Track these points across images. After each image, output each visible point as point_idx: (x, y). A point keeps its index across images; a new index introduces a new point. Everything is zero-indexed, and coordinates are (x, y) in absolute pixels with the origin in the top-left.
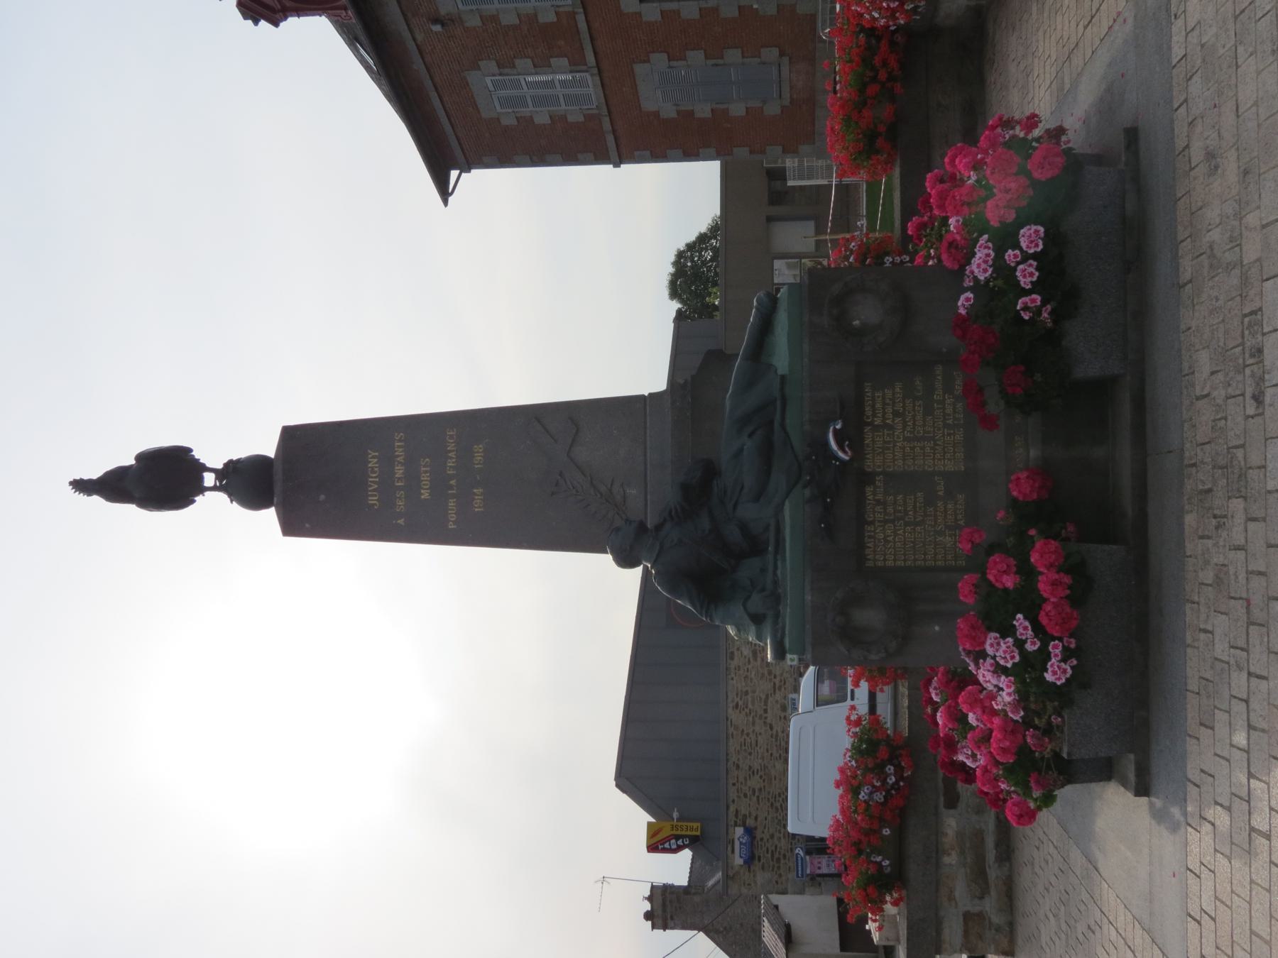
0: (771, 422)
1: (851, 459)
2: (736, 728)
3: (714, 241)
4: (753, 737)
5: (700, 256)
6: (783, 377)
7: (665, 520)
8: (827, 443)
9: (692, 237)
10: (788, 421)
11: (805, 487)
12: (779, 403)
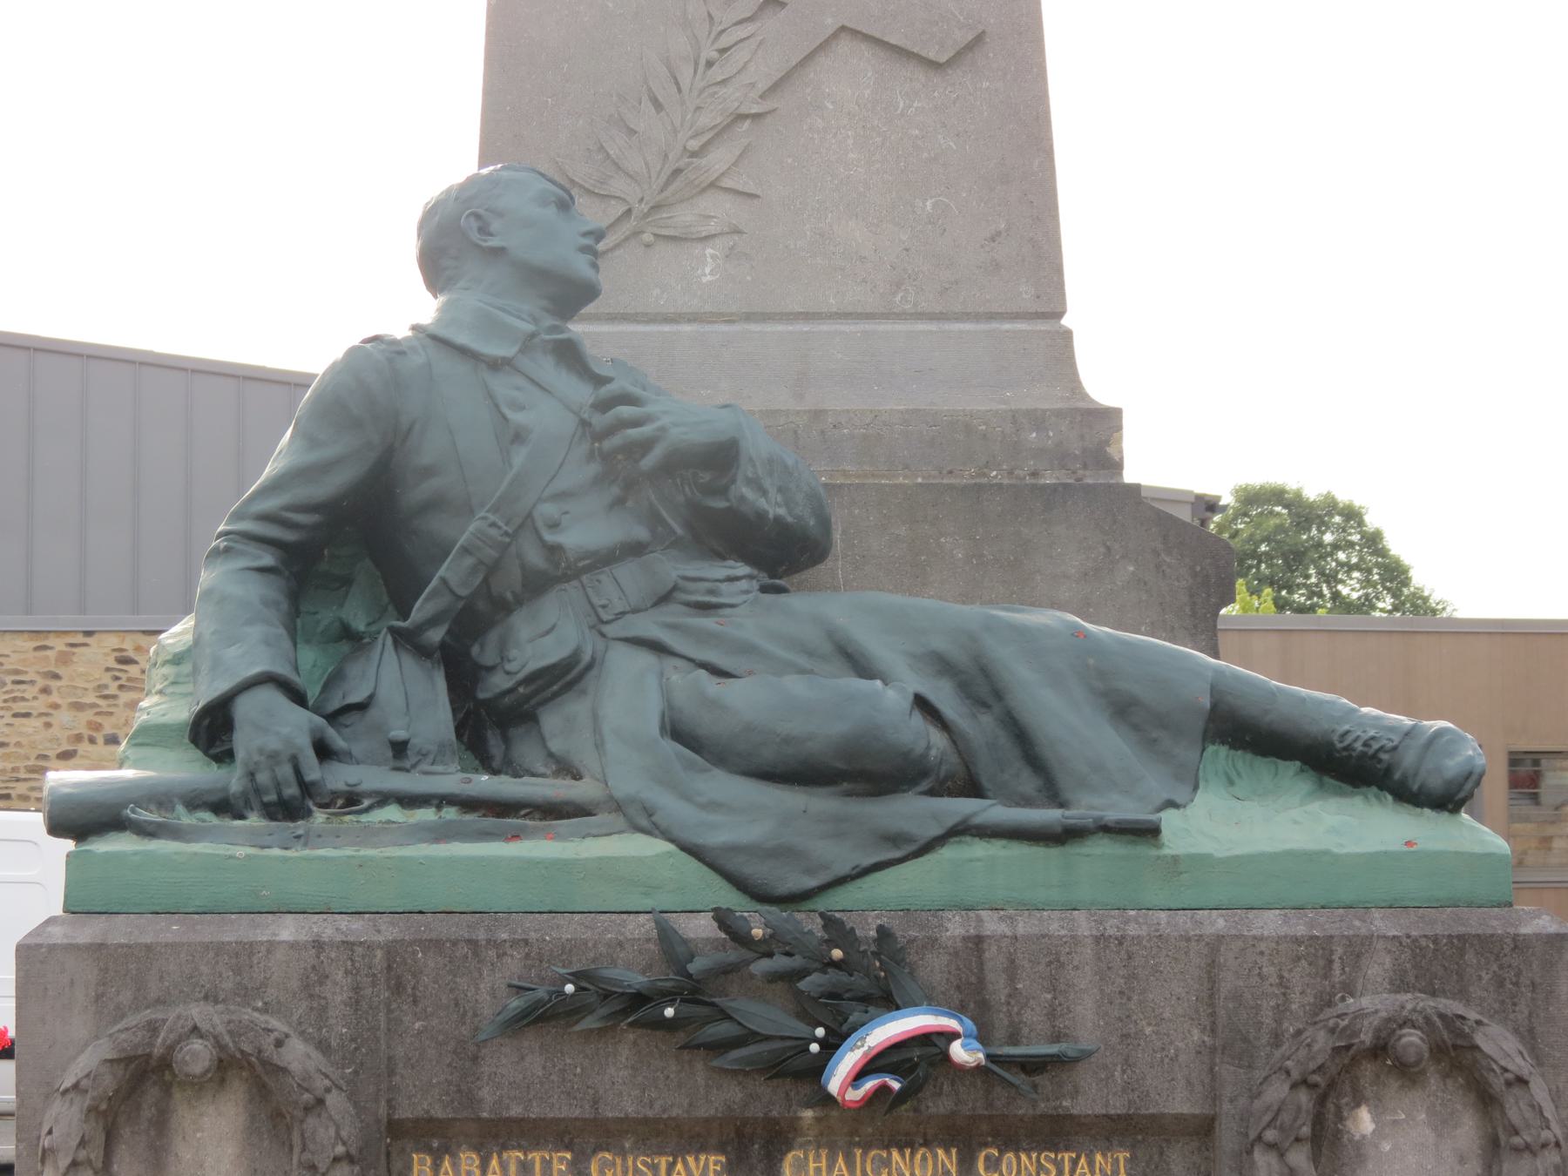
0: (972, 788)
1: (828, 1100)
2: (64, 659)
3: (1387, 602)
4: (40, 705)
5: (1351, 568)
6: (1148, 832)
7: (600, 381)
8: (888, 1002)
9: (1396, 545)
10: (979, 849)
11: (722, 918)
12: (1047, 816)
